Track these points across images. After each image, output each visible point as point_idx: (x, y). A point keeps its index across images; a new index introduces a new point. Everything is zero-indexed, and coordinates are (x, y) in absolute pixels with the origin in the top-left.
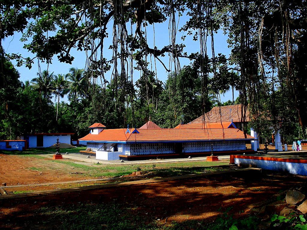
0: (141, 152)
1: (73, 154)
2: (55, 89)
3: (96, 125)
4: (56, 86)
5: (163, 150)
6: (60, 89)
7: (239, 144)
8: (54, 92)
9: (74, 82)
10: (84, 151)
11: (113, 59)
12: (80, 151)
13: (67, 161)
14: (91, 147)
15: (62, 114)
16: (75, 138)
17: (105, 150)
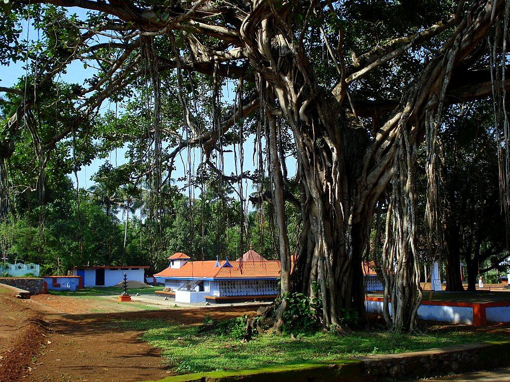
0: (235, 292)
1: (145, 296)
2: (123, 201)
3: (177, 255)
4: (125, 198)
5: (264, 290)
6: (129, 201)
7: (375, 281)
8: (121, 205)
9: (149, 190)
10: (161, 292)
11: (185, 187)
12: (156, 292)
13: (138, 303)
14: (170, 285)
15: (132, 238)
16: (149, 273)
17: (189, 290)
